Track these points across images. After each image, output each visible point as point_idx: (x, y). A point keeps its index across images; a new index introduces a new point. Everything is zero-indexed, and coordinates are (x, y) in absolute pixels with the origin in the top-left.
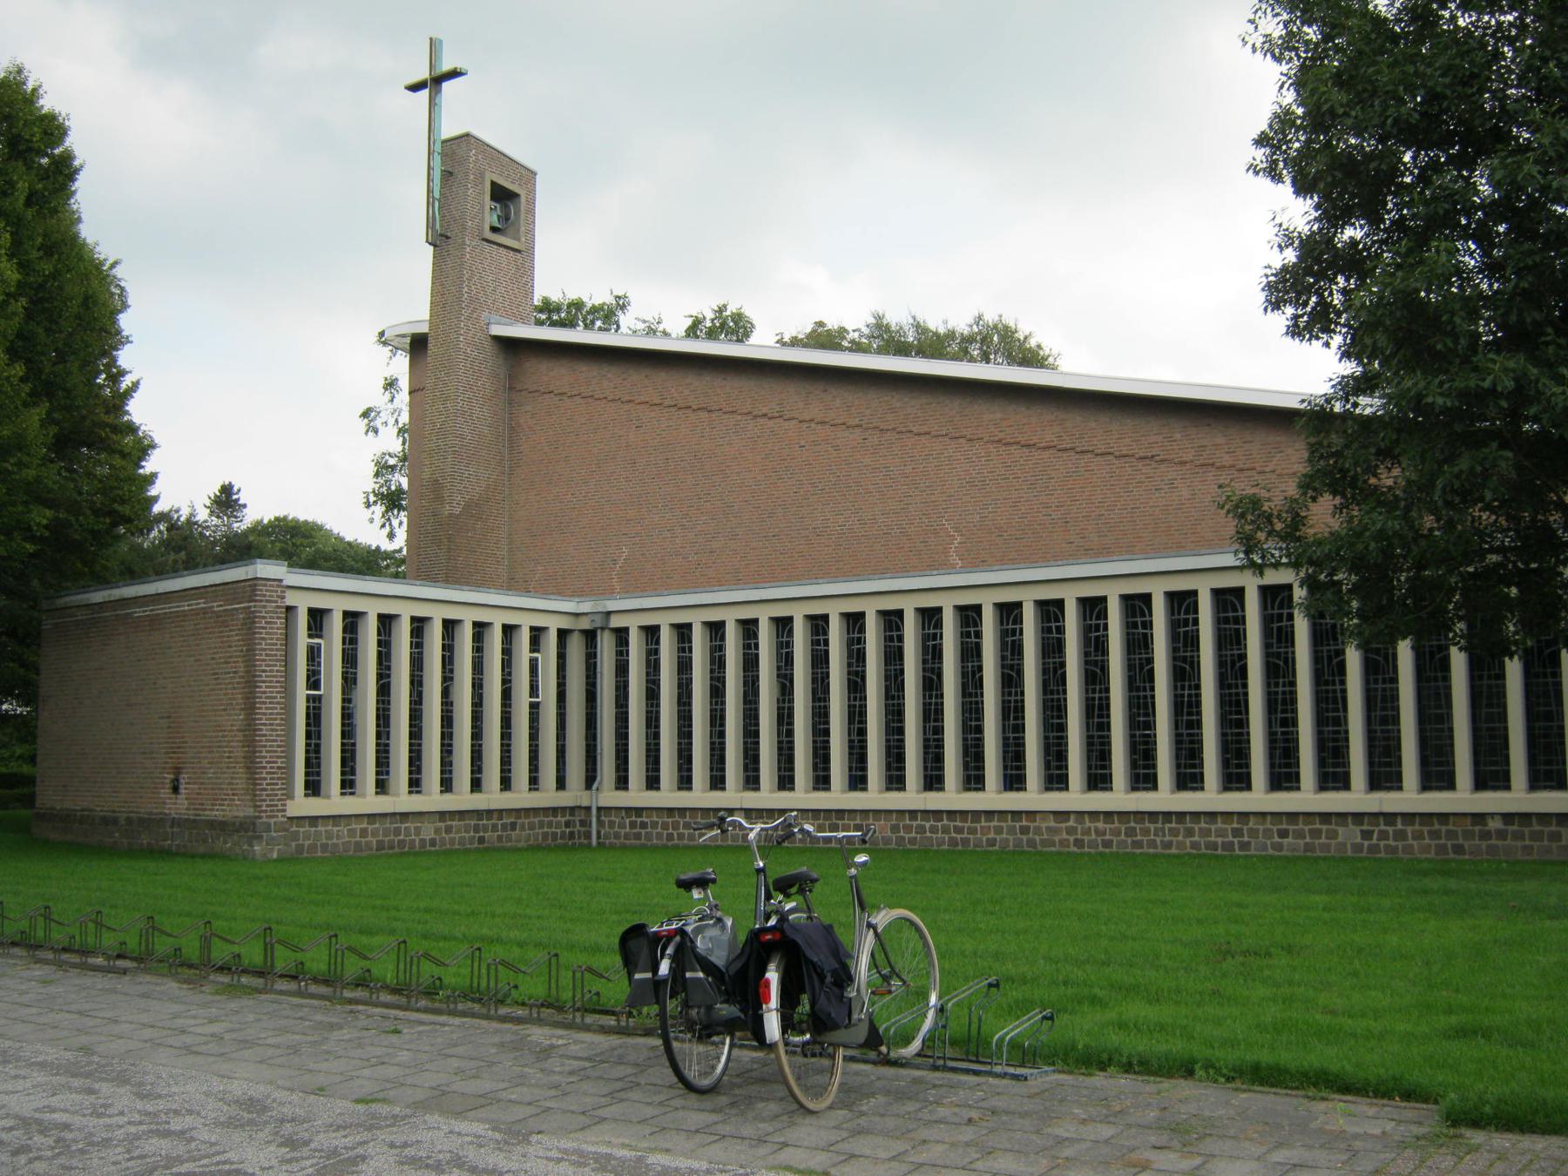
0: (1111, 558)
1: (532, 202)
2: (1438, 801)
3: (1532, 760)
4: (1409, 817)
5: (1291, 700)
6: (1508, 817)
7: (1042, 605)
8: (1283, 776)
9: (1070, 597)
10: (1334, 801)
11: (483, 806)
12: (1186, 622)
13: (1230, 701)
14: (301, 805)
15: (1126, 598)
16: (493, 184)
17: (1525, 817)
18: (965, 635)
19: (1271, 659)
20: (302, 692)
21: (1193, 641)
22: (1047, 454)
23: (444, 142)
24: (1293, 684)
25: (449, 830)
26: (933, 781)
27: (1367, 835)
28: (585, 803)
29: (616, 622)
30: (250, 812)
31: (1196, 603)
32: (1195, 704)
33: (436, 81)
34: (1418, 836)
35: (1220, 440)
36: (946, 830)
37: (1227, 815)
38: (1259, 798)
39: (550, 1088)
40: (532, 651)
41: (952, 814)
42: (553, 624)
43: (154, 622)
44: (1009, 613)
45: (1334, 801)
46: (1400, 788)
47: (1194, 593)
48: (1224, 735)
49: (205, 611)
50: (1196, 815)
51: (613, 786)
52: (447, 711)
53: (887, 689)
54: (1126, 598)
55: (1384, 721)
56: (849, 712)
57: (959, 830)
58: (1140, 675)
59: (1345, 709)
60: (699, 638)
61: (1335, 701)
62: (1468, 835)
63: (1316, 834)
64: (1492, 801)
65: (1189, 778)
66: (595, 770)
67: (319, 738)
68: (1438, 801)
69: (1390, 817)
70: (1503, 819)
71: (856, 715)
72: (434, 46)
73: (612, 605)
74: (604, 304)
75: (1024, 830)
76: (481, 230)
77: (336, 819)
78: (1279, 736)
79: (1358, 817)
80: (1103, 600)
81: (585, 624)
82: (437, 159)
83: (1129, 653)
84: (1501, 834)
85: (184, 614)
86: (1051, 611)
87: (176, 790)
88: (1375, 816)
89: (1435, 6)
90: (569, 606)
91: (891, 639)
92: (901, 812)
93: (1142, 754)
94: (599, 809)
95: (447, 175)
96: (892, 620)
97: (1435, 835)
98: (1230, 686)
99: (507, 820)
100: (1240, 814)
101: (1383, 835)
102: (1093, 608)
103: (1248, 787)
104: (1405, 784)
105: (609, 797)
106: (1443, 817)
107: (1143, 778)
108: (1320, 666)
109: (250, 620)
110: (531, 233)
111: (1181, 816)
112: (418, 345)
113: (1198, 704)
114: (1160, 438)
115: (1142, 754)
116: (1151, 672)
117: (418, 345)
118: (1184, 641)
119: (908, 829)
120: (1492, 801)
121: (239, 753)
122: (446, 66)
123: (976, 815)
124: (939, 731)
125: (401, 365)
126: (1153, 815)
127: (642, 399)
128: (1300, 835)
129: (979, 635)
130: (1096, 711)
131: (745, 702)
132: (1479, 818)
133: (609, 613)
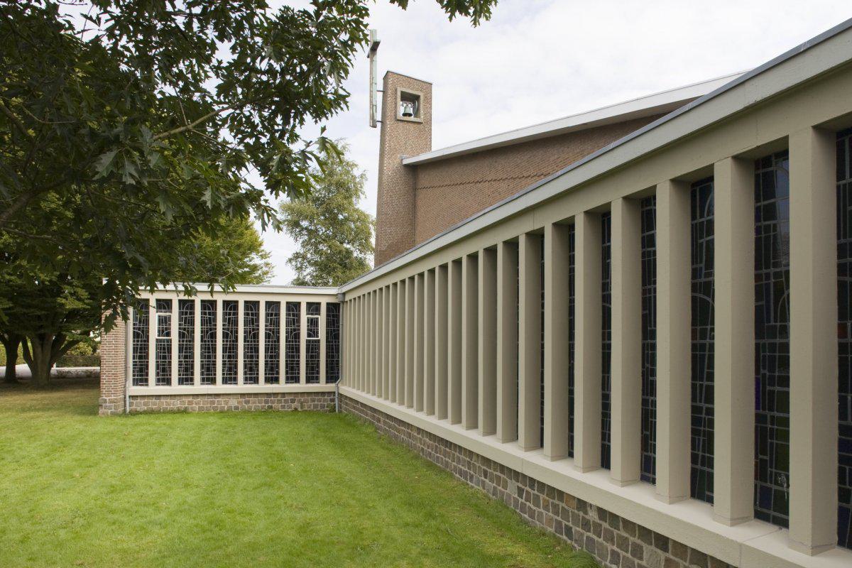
0: (402, 255)
7: (268, 304)
13: (248, 348)
19: (698, 295)
31: (250, 302)
38: (198, 387)
39: (26, 383)
52: (703, 347)
56: (694, 358)
58: (354, 329)
67: (171, 359)
70: (598, 511)
74: (249, 216)
78: (183, 363)
89: (117, 282)
98: (205, 341)
108: (763, 303)
131: (759, 332)
133: (344, 294)
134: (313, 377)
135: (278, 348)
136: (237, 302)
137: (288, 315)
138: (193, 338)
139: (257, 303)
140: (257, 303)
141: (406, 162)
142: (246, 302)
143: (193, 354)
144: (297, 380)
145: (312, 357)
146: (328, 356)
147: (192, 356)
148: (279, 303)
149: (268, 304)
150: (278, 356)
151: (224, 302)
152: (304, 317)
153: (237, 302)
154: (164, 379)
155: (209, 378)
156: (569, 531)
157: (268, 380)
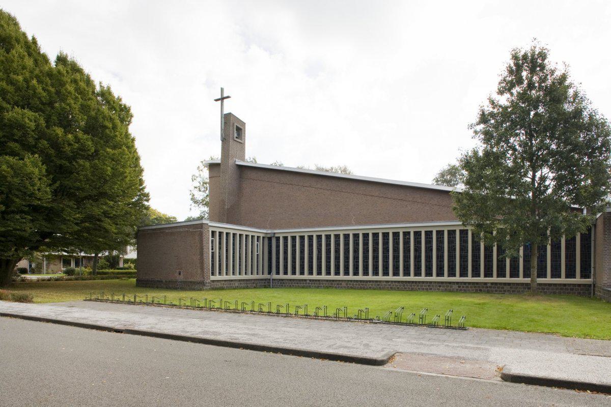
1: (245, 131)
2: (476, 279)
3: (449, 271)
4: (469, 283)
5: (398, 257)
6: (492, 284)
12: (357, 240)
14: (212, 278)
15: (363, 234)
16: (237, 126)
17: (496, 284)
18: (309, 242)
20: (211, 251)
21: (420, 243)
22: (376, 198)
23: (224, 115)
24: (378, 254)
25: (241, 284)
26: (337, 273)
27: (459, 287)
28: (269, 278)
29: (277, 235)
30: (202, 279)
32: (420, 257)
33: (222, 99)
34: (471, 287)
36: (359, 285)
37: (427, 282)
40: (257, 242)
41: (361, 281)
42: (262, 236)
43: (172, 234)
46: (421, 276)
47: (340, 235)
48: (426, 264)
49: (187, 231)
50: (419, 282)
53: (309, 253)
54: (363, 234)
55: (397, 262)
58: (366, 251)
59: (410, 259)
61: (408, 257)
62: (483, 287)
63: (448, 286)
65: (319, 273)
66: (271, 270)
68: (476, 279)
69: (465, 283)
71: (286, 259)
72: (222, 90)
73: (276, 231)
75: (378, 285)
76: (233, 138)
77: (218, 281)
79: (457, 283)
80: (321, 235)
81: (269, 236)
82: (223, 119)
83: (383, 245)
84: (490, 287)
87: (180, 274)
88: (461, 283)
90: (265, 231)
91: (293, 242)
92: (348, 281)
94: (273, 279)
95: (225, 123)
96: (294, 238)
97: (475, 287)
99: (253, 282)
100: (430, 282)
101: (463, 287)
102: (328, 237)
103: (349, 275)
104: (469, 276)
105: (275, 276)
106: (477, 283)
107: (407, 273)
109: (201, 234)
110: (245, 139)
112: (213, 166)
113: (378, 257)
114: (403, 195)
116: (368, 250)
117: (213, 166)
119: (350, 284)
121: (199, 265)
122: (225, 95)
124: (321, 262)
125: (206, 173)
126: (409, 282)
127: (275, 181)
128: (443, 287)
129: (296, 242)
130: (376, 258)
132: (486, 283)
133: (275, 233)
141: (237, 163)
151: (437, 231)
157: (582, 276)
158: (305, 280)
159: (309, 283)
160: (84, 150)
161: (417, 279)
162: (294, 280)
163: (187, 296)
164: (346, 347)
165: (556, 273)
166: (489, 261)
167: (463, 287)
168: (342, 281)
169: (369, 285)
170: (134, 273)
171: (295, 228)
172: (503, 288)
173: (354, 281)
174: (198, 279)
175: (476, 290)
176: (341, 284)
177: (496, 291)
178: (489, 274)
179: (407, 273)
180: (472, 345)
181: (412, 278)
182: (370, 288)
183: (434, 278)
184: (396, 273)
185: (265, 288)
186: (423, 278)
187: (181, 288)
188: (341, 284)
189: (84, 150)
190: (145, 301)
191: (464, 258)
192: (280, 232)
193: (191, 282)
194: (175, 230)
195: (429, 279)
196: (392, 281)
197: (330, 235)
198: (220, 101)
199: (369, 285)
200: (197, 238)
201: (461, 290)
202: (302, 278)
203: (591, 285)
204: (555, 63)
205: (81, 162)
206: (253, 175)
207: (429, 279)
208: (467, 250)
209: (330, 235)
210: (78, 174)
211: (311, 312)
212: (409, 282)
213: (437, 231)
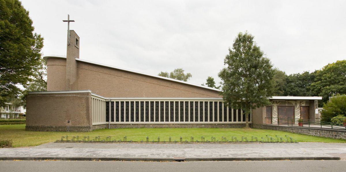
6: (218, 124)
7: (146, 102)
8: (137, 120)
9: (125, 101)
10: (201, 123)
11: (113, 123)
15: (126, 102)
17: (219, 124)
21: (141, 107)
27: (205, 126)
29: (112, 101)
30: (88, 125)
31: (162, 102)
33: (69, 21)
34: (210, 126)
35: (175, 85)
37: (191, 124)
44: (201, 103)
45: (201, 123)
47: (129, 102)
51: (105, 120)
54: (126, 102)
57: (161, 126)
58: (211, 110)
60: (110, 104)
63: (200, 126)
64: (216, 123)
75: (169, 126)
84: (217, 126)
85: (70, 97)
86: (167, 103)
93: (230, 118)
101: (207, 126)
107: (211, 120)
111: (186, 124)
115: (230, 118)
118: (216, 107)
120: (216, 123)
123: (163, 124)
133: (111, 100)
134: (157, 120)
135: (158, 113)
136: (158, 102)
137: (180, 105)
138: (178, 110)
139: (173, 102)
140: (173, 102)
142: (131, 102)
143: (168, 114)
144: (153, 121)
145: (177, 115)
146: (200, 115)
147: (148, 115)
148: (168, 102)
149: (166, 102)
150: (168, 115)
151: (166, 102)
152: (223, 105)
153: (148, 102)
154: (137, 120)
155: (132, 120)
156: (213, 127)
158: (130, 124)
159: (132, 126)
160: (11, 35)
161: (187, 123)
162: (123, 124)
163: (81, 136)
164: (256, 153)
165: (132, 120)
166: (172, 115)
167: (207, 126)
168: (150, 124)
169: (165, 126)
170: (25, 121)
171: (101, 96)
172: (222, 126)
173: (157, 124)
174: (85, 125)
175: (212, 127)
176: (150, 126)
177: (219, 127)
178: (157, 120)
179: (221, 120)
180: (331, 149)
181: (184, 122)
182: (165, 127)
183: (194, 122)
184: (235, 120)
185: (56, 131)
186: (189, 122)
187: (70, 131)
188: (150, 126)
189: (11, 35)
190: (66, 140)
191: (167, 113)
192: (115, 99)
193: (79, 127)
194: (65, 96)
195: (192, 123)
196: (175, 124)
197: (217, 102)
198: (67, 22)
199: (165, 126)
200: (84, 101)
201: (206, 127)
202: (122, 123)
203: (251, 124)
204: (257, 42)
205: (11, 43)
206: (86, 67)
207: (192, 123)
208: (159, 110)
209: (217, 102)
210: (8, 51)
211: (189, 140)
212: (183, 124)
213: (166, 102)
